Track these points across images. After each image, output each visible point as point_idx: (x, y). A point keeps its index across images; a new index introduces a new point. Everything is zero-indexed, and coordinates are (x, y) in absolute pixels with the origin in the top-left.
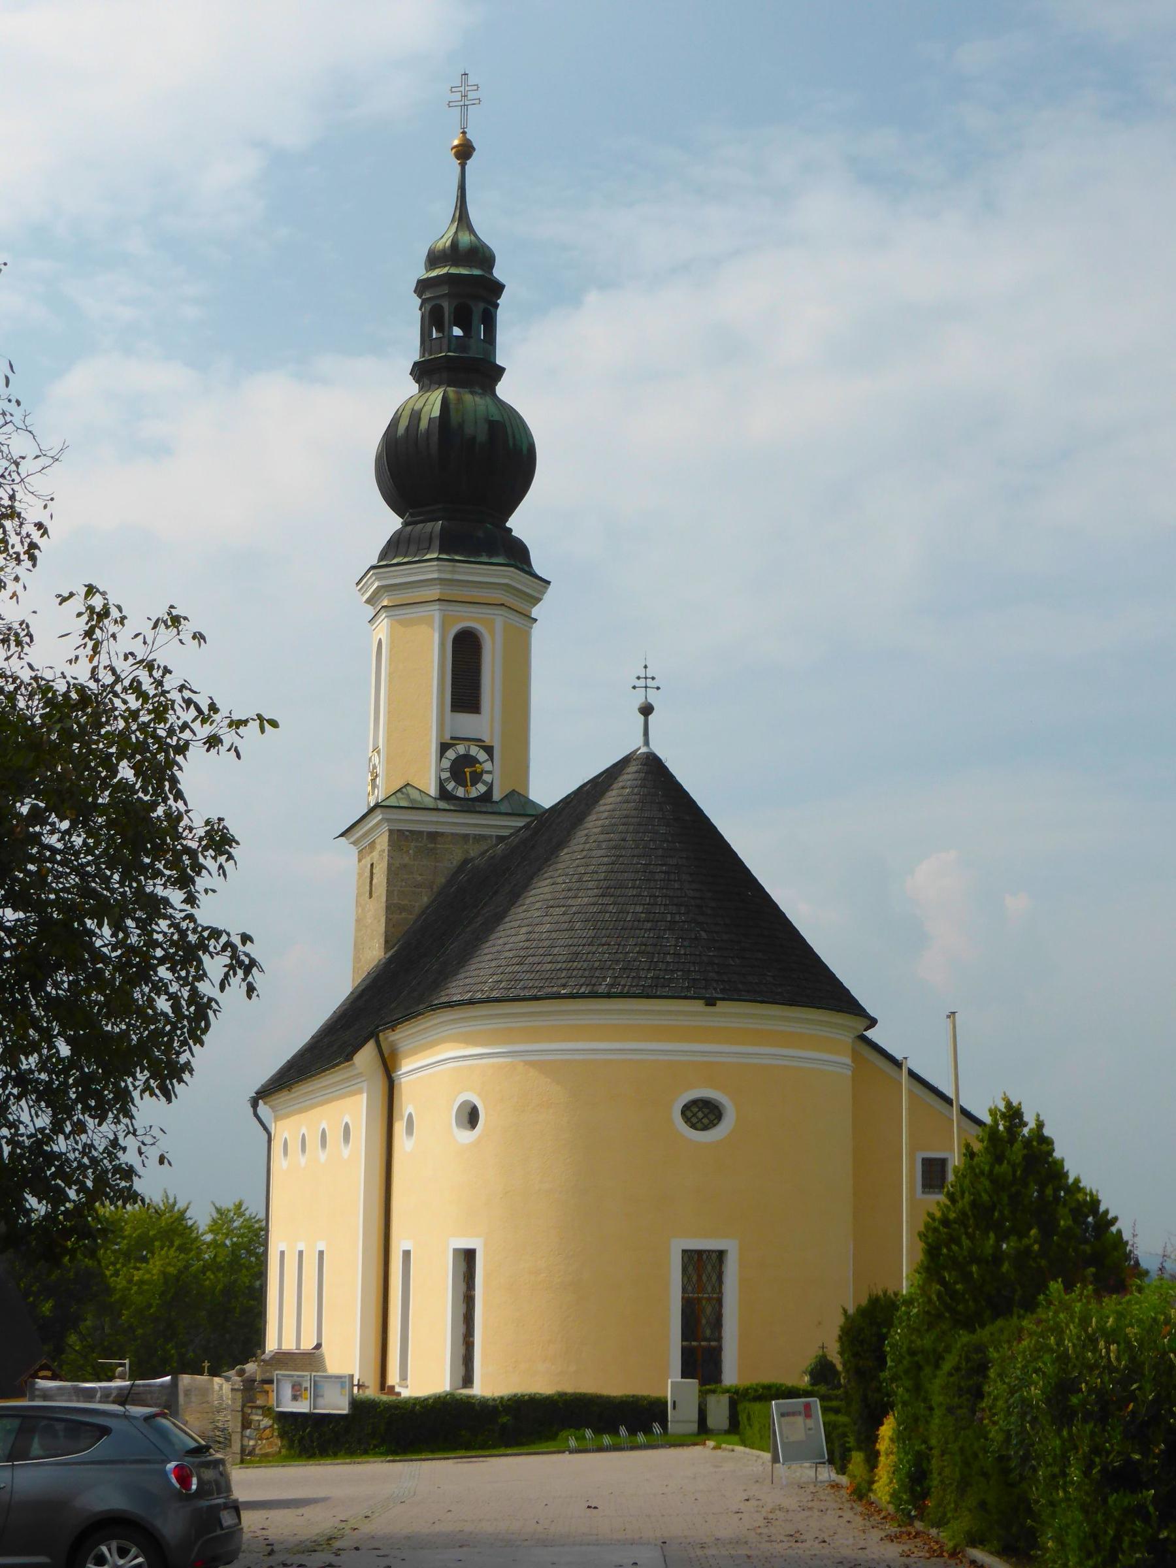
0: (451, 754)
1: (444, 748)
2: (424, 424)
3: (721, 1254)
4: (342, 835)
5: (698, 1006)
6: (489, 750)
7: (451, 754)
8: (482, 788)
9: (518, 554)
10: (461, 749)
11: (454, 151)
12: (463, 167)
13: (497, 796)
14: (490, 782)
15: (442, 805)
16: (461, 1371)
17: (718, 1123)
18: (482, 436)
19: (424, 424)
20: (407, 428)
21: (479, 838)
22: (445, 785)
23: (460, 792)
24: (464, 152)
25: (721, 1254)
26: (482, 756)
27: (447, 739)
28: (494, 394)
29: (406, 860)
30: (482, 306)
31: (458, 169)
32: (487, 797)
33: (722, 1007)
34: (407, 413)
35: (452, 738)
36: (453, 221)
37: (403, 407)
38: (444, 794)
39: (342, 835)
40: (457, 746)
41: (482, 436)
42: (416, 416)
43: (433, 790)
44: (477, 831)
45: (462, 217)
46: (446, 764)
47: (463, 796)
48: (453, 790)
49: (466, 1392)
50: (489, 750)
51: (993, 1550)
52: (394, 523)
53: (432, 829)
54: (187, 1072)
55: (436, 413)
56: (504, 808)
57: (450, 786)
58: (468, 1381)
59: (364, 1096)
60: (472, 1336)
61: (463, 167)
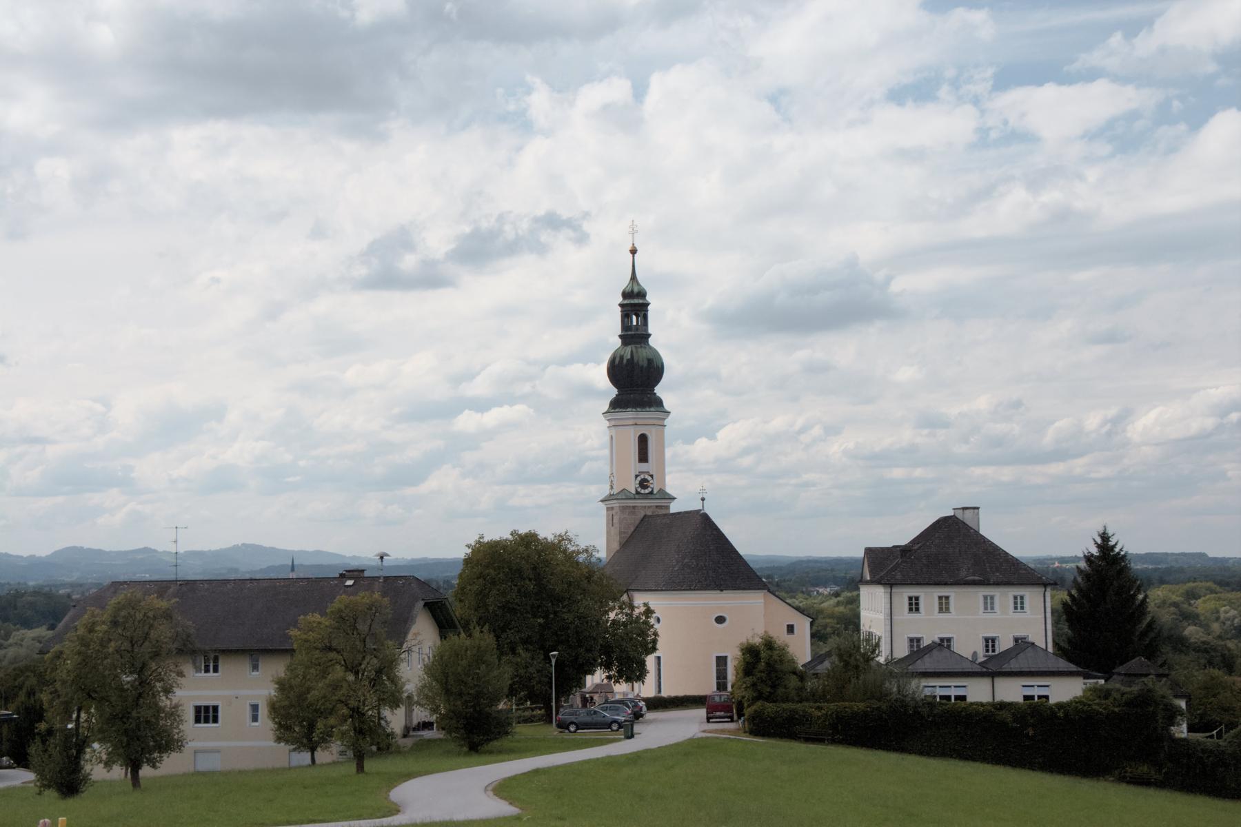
0: (639, 478)
2: (625, 361)
3: (726, 657)
5: (719, 592)
6: (652, 476)
7: (639, 478)
8: (650, 490)
9: (659, 403)
10: (642, 476)
12: (633, 257)
13: (655, 492)
15: (637, 496)
16: (658, 689)
18: (645, 364)
19: (625, 361)
20: (619, 361)
21: (649, 507)
23: (643, 491)
25: (726, 657)
26: (649, 478)
27: (638, 474)
28: (648, 345)
29: (625, 516)
30: (643, 313)
31: (632, 257)
32: (651, 493)
33: (724, 592)
34: (618, 356)
35: (639, 472)
38: (638, 493)
41: (645, 364)
42: (622, 358)
43: (634, 492)
44: (648, 505)
45: (633, 244)
46: (638, 482)
49: (660, 695)
50: (652, 476)
51: (547, 665)
53: (634, 505)
55: (629, 357)
56: (657, 496)
57: (639, 489)
58: (660, 691)
59: (602, 554)
61: (633, 257)
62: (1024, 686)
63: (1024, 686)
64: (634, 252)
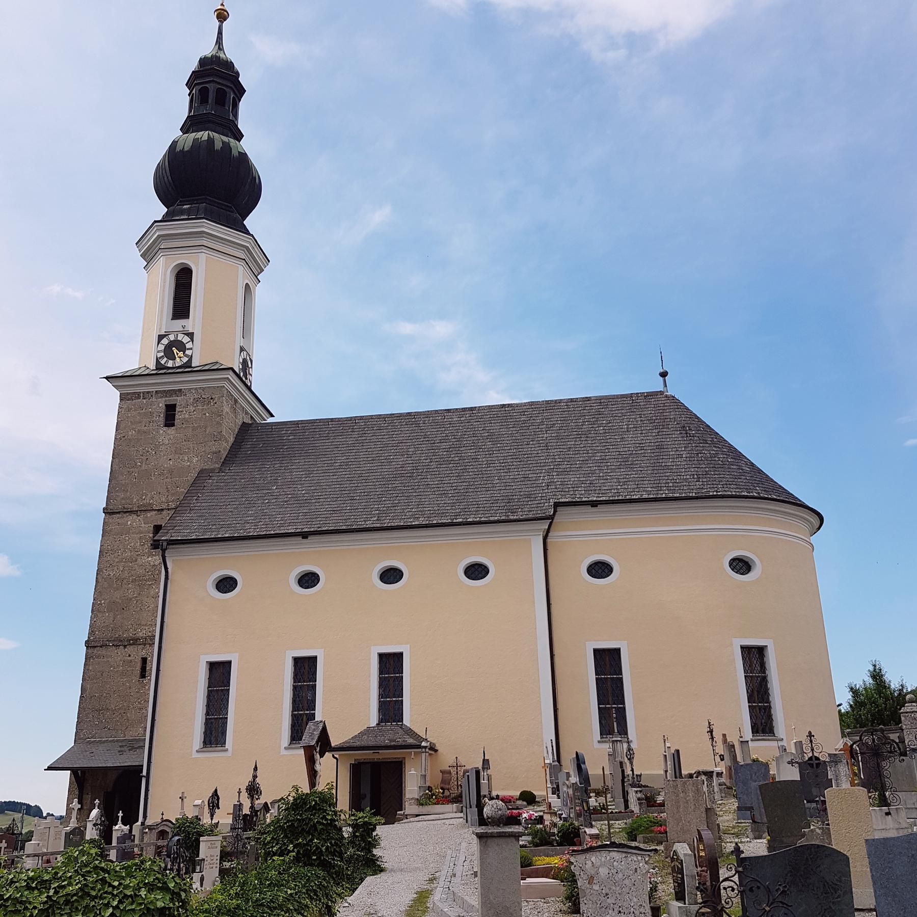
0: (165, 341)
1: (161, 338)
4: (107, 378)
7: (165, 341)
10: (172, 337)
11: (216, 13)
14: (190, 354)
17: (484, 565)
22: (160, 360)
23: (170, 364)
24: (222, 16)
26: (186, 339)
32: (188, 365)
36: (216, 44)
37: (179, 138)
38: (159, 366)
39: (107, 378)
40: (169, 336)
46: (161, 347)
47: (171, 366)
48: (165, 363)
52: (161, 210)
54: (178, 149)
60: (149, 747)
62: (551, 740)
63: (551, 740)
64: (222, 16)
